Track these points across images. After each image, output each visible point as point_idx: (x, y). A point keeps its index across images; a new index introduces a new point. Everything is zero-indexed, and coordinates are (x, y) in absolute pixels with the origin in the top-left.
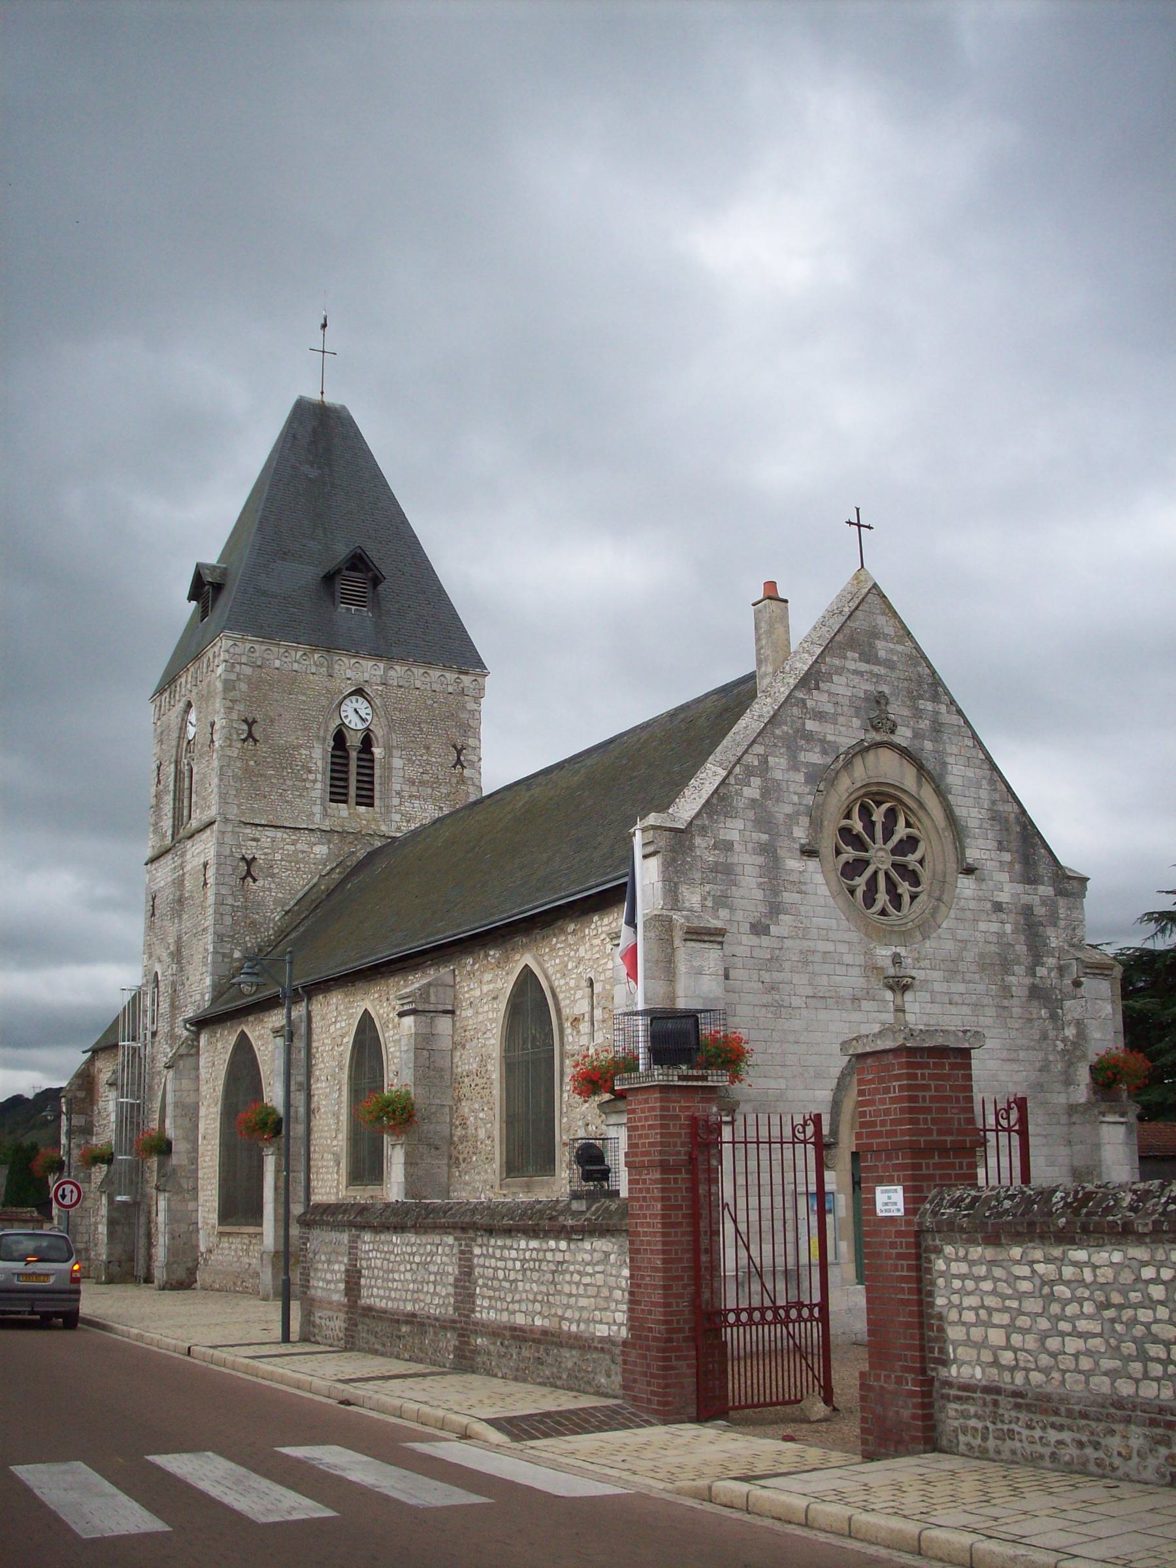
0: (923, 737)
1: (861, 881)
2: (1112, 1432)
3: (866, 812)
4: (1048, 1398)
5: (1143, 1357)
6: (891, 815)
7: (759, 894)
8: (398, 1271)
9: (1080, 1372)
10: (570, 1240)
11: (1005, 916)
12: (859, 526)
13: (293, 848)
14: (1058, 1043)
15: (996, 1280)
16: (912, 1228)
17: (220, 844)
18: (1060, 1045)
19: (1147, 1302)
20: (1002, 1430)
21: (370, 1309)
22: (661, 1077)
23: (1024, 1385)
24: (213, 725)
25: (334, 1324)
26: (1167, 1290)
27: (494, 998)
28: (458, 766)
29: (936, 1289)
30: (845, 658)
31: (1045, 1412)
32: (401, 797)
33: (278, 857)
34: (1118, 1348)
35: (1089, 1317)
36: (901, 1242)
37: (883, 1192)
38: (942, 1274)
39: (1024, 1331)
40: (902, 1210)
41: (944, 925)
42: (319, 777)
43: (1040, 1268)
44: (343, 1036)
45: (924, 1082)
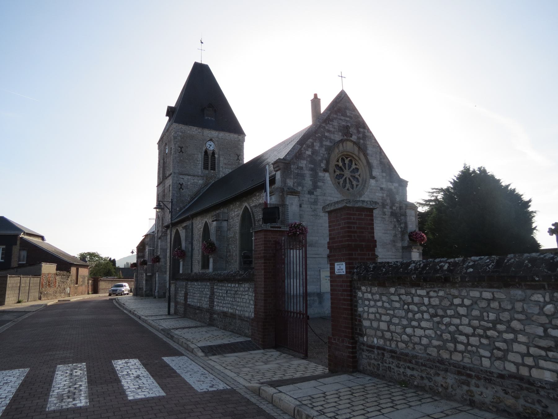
0: (360, 139)
1: (341, 181)
2: (438, 375)
3: (343, 160)
4: (407, 355)
5: (455, 341)
6: (351, 161)
7: (310, 183)
8: (196, 293)
9: (421, 345)
10: (239, 284)
11: (383, 192)
12: (342, 77)
13: (193, 181)
14: (399, 229)
15: (383, 302)
16: (349, 279)
17: (173, 180)
18: (400, 229)
19: (456, 315)
20: (386, 366)
21: (189, 305)
22: (264, 227)
23: (395, 348)
24: (171, 148)
25: (181, 309)
26: (467, 310)
27: (238, 216)
28: (238, 160)
29: (359, 304)
30: (337, 115)
31: (405, 361)
32: (223, 168)
33: (189, 183)
34: (441, 335)
35: (427, 320)
36: (344, 285)
37: (337, 265)
38: (361, 298)
39: (396, 325)
40: (345, 272)
41: (366, 193)
42: (200, 162)
43: (404, 297)
44: (200, 229)
45: (354, 221)
